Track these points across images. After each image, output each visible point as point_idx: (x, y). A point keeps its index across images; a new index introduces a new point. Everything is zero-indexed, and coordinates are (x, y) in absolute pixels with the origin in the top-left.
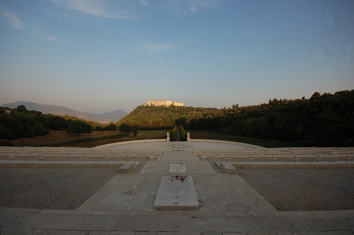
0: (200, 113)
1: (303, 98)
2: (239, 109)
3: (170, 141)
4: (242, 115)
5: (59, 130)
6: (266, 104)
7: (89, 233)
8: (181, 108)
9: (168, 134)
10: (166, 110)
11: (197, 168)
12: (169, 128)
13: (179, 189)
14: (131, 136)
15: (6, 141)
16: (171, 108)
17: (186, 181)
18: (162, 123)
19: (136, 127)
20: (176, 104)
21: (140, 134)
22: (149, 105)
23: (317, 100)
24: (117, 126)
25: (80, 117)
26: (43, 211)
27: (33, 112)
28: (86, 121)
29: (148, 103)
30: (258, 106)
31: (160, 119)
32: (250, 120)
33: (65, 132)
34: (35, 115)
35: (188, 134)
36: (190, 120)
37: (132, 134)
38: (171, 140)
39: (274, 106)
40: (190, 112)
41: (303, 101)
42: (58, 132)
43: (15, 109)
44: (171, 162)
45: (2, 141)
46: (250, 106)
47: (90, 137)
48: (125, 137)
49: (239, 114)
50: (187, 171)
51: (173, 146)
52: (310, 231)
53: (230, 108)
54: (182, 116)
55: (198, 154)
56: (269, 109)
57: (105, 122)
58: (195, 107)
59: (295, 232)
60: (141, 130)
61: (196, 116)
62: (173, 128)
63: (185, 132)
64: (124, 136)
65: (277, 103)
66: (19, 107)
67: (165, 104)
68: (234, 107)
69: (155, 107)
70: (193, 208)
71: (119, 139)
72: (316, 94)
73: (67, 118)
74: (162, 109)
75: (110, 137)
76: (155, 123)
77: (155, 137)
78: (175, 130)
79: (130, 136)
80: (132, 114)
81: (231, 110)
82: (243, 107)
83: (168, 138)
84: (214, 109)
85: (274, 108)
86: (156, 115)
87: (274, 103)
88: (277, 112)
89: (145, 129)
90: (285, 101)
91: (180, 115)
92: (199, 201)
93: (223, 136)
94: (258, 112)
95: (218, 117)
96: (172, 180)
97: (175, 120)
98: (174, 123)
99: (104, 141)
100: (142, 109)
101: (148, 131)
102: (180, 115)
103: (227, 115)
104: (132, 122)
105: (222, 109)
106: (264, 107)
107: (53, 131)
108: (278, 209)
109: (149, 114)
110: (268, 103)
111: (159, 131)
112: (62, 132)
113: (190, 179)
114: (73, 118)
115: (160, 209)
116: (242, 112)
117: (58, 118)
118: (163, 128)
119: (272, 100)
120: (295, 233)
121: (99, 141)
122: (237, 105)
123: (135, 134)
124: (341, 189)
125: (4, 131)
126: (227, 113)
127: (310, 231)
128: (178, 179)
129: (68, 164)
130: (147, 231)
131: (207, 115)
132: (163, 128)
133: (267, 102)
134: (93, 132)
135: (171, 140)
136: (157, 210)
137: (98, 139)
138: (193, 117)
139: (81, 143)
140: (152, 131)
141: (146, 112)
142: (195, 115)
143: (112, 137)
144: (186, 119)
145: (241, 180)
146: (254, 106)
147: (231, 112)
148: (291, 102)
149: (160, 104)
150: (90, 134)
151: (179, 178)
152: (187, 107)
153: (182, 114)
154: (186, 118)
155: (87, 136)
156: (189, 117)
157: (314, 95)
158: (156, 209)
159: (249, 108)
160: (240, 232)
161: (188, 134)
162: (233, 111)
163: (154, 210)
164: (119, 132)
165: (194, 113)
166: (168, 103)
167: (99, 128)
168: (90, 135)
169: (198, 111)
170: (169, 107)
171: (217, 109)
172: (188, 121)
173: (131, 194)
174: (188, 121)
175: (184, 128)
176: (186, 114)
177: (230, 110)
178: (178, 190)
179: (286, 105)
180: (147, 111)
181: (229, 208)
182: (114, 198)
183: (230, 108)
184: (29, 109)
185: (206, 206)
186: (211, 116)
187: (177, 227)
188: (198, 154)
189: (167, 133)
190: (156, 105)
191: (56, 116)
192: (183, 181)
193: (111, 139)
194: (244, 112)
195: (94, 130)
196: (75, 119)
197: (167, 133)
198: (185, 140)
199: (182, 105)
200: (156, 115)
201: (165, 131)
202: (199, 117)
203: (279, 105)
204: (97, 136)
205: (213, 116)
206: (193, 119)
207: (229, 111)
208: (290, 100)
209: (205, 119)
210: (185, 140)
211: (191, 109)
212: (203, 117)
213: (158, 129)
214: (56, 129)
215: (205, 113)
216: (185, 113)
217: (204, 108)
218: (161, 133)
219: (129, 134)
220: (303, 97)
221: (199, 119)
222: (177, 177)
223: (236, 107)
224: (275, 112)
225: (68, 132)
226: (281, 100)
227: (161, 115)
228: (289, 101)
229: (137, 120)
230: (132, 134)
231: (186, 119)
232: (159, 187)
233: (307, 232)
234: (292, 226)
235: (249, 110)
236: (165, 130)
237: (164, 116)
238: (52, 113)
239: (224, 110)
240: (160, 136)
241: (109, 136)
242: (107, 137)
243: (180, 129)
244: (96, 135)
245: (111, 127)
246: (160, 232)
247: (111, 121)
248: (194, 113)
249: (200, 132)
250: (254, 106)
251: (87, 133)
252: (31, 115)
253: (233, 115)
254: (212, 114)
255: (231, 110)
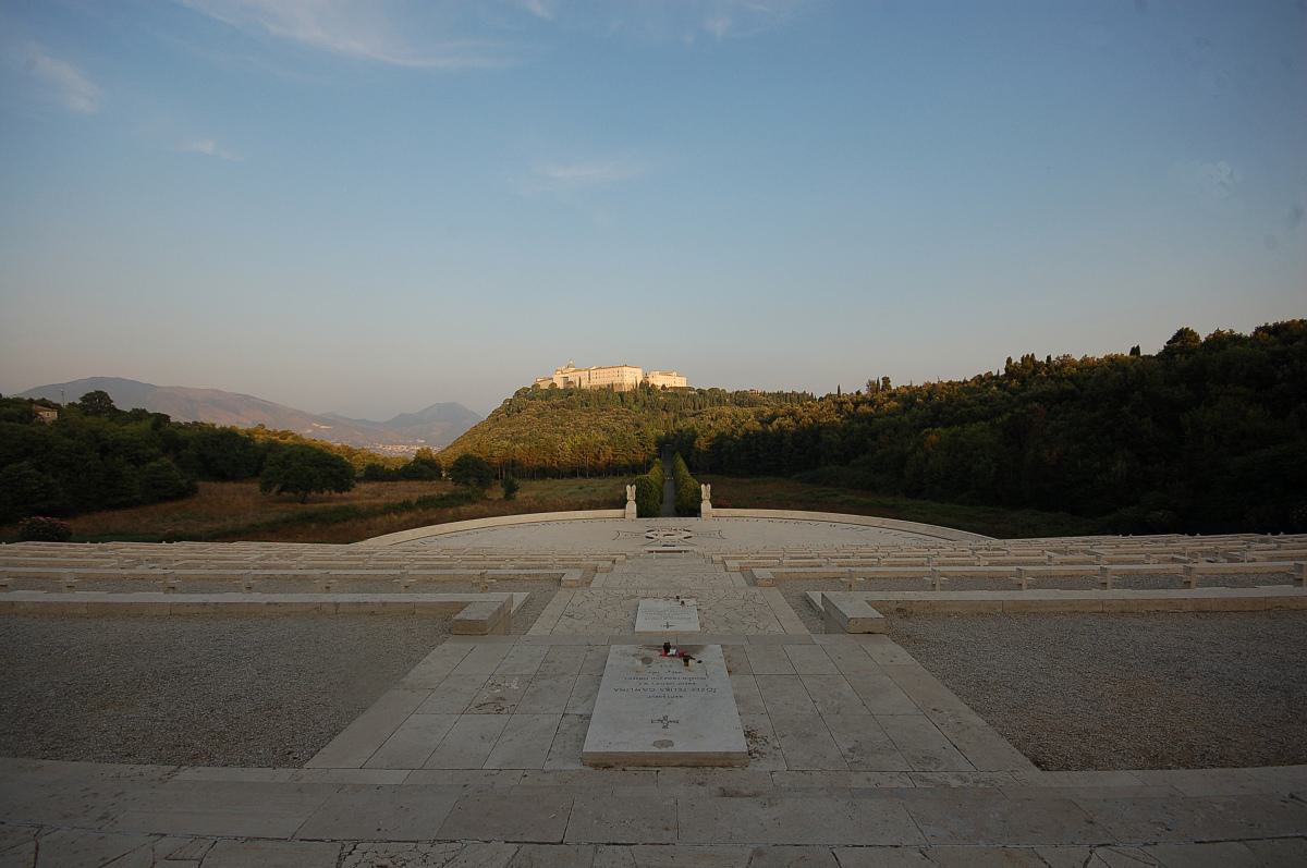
0: (749, 410)
1: (1135, 351)
2: (892, 396)
3: (638, 517)
4: (906, 418)
5: (234, 479)
6: (995, 374)
7: (354, 849)
8: (677, 393)
9: (631, 491)
10: (622, 400)
11: (738, 613)
12: (635, 470)
13: (671, 694)
14: (496, 498)
15: (43, 523)
16: (641, 395)
17: (700, 662)
18: (609, 450)
19: (513, 466)
20: (658, 380)
21: (528, 490)
22: (560, 385)
23: (1186, 358)
24: (443, 464)
25: (309, 431)
26: (187, 774)
27: (139, 415)
28: (329, 447)
29: (555, 377)
30: (965, 382)
31: (601, 438)
32: (936, 435)
33: (255, 487)
34: (146, 425)
35: (705, 490)
36: (712, 440)
37: (497, 493)
38: (640, 515)
39: (1023, 381)
40: (709, 409)
41: (1133, 361)
42: (229, 486)
43: (73, 405)
44: (642, 593)
45: (28, 522)
46: (934, 385)
47: (345, 503)
48: (475, 502)
49: (893, 415)
50: (702, 626)
51: (650, 534)
52: (1156, 844)
53: (858, 393)
54: (680, 424)
55: (740, 563)
56: (1006, 393)
57: (400, 450)
58: (728, 391)
59: (1099, 846)
60: (532, 477)
61: (733, 422)
62: (649, 469)
63: (692, 482)
64: (468, 499)
65: (1034, 372)
66: (88, 398)
67: (617, 381)
68: (873, 387)
69: (581, 391)
70: (726, 761)
71: (450, 512)
72: (1184, 335)
73: (261, 437)
74: (608, 397)
75: (418, 502)
76: (582, 449)
77: (581, 501)
78: (654, 474)
79: (490, 500)
80: (495, 417)
81: (864, 398)
82: (908, 388)
83: (632, 507)
84: (798, 395)
85: (1025, 390)
86: (584, 422)
87: (1025, 372)
88: (1036, 405)
89: (543, 473)
90: (1066, 362)
91: (675, 421)
92: (748, 734)
93: (835, 495)
94: (965, 405)
95: (816, 426)
96: (646, 660)
97: (657, 436)
98: (654, 448)
99: (396, 517)
100: (534, 399)
101: (556, 480)
102: (675, 421)
103: (848, 418)
104: (498, 447)
105: (829, 396)
106: (985, 387)
107: (213, 484)
108: (1038, 764)
109: (559, 418)
110: (1002, 372)
111: (596, 482)
112: (244, 486)
113: (713, 655)
114: (284, 435)
115: (604, 763)
116: (905, 409)
117: (228, 437)
118: (613, 470)
119: (1017, 359)
120: (1102, 848)
121: (379, 519)
122: (886, 380)
123: (511, 490)
124: (1275, 688)
125: (34, 488)
126: (849, 413)
127: (1156, 844)
128: (672, 655)
129: (268, 604)
130: (562, 842)
131: (774, 417)
132: (613, 470)
133: (999, 369)
134: (357, 485)
135: (640, 515)
136: (596, 766)
137: (373, 512)
138: (723, 426)
139: (313, 526)
140: (571, 481)
141: (549, 410)
142: (729, 421)
143: (425, 503)
144: (695, 436)
145: (903, 656)
146: (950, 383)
147: (864, 408)
148: (1087, 366)
149: (601, 379)
150: (345, 494)
151: (673, 651)
152: (701, 392)
153: (682, 416)
154: (695, 432)
155: (335, 500)
156: (707, 427)
157: (1175, 339)
158: (591, 765)
159: (931, 390)
160: (897, 847)
161: (705, 490)
162: (871, 403)
163: (582, 767)
164: (450, 485)
165: (727, 410)
166: (630, 378)
167: (377, 473)
168: (346, 499)
169: (740, 405)
170: (634, 392)
171: (811, 398)
172: (702, 443)
173: (499, 712)
174: (702, 443)
175: (690, 468)
176: (694, 415)
177: (858, 400)
178: (671, 694)
179: (1071, 378)
180: (553, 406)
181: (856, 758)
182: (438, 721)
183: (858, 393)
184: (124, 404)
185: (774, 752)
186: (789, 421)
187: (667, 829)
188: (740, 563)
189: (628, 486)
190: (584, 384)
191: (224, 429)
192: (686, 661)
193: (420, 510)
194: (912, 405)
195: (358, 480)
196: (289, 440)
197: (628, 486)
198: (695, 512)
199: (681, 382)
200: (584, 422)
201: (619, 480)
202: (746, 426)
203: (1041, 378)
204: (373, 501)
205: (798, 422)
206: (721, 436)
207: (856, 405)
208: (1085, 359)
209: (765, 434)
210: (695, 512)
211: (716, 397)
212: (757, 426)
213: (596, 472)
214: (222, 477)
215: (768, 412)
216: (692, 411)
217: (764, 394)
218: (604, 486)
219: (487, 491)
220: (1133, 349)
221: (746, 435)
222: (667, 648)
223: (880, 388)
224: (1029, 406)
225: (266, 488)
226: (1049, 358)
227: (603, 420)
228: (1082, 361)
229: (517, 441)
230: (497, 493)
231: (695, 436)
232: (599, 685)
233: (1146, 844)
234: (1091, 822)
235: (930, 397)
236: (621, 475)
237: (617, 425)
238: (206, 418)
239: (837, 401)
240: (603, 499)
241: (414, 502)
242: (406, 506)
243: (674, 472)
244: (366, 498)
245: (422, 468)
246: (608, 844)
247: (420, 444)
248: (727, 410)
249: (747, 480)
250: (947, 384)
251: (333, 492)
252: (132, 427)
253: (869, 418)
254: (792, 414)
255: (864, 400)
